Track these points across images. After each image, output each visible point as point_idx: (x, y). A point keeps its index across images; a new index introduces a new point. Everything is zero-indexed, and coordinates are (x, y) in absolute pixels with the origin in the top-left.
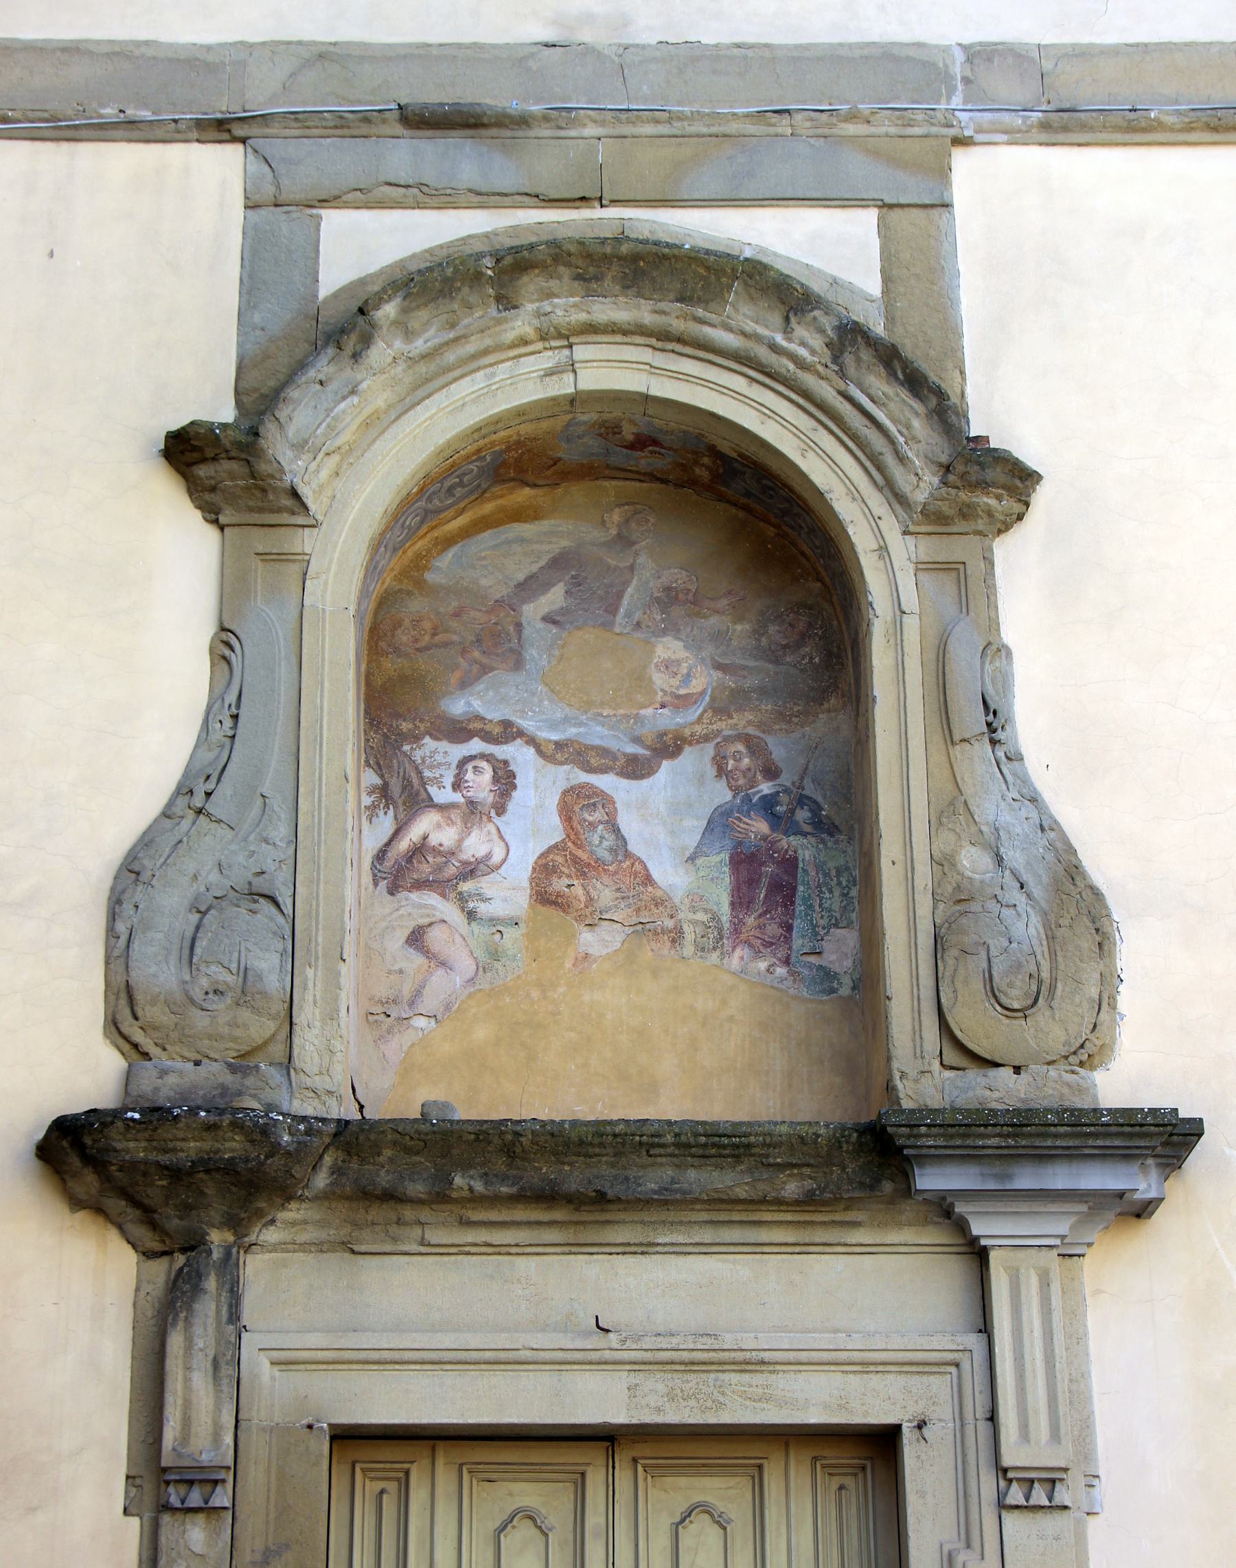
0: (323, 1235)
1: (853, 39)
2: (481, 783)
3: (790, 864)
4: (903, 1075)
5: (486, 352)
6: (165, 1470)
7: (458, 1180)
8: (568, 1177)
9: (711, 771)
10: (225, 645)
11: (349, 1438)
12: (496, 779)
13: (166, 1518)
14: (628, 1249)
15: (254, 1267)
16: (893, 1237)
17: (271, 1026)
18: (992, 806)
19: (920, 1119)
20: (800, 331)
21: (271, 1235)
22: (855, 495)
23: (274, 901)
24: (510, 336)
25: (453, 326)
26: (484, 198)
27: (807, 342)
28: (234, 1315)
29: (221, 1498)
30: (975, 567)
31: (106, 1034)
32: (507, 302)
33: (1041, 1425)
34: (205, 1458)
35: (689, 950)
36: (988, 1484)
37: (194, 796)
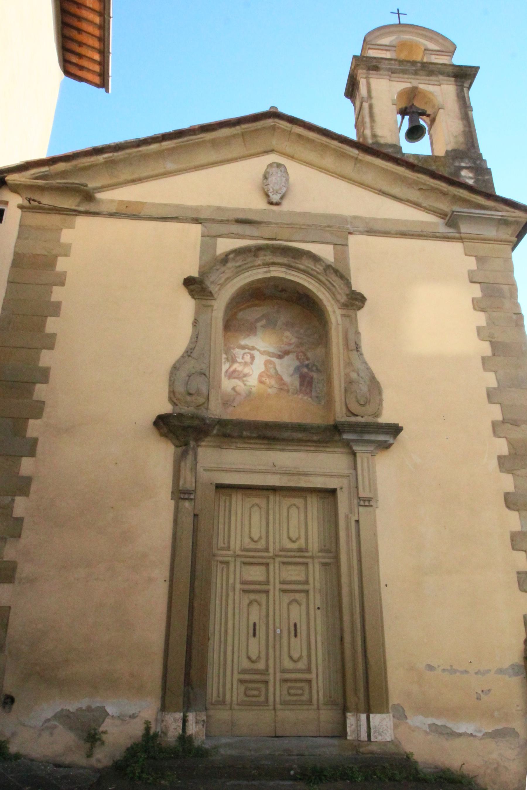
0: (215, 444)
1: (327, 213)
2: (248, 358)
3: (312, 378)
4: (338, 417)
5: (252, 267)
6: (180, 490)
7: (245, 433)
8: (268, 434)
9: (295, 358)
10: (195, 323)
11: (220, 487)
12: (251, 357)
13: (180, 500)
14: (280, 450)
15: (200, 450)
16: (336, 450)
17: (204, 400)
18: (357, 364)
19: (343, 424)
20: (318, 266)
21: (203, 444)
22: (329, 301)
23: (205, 375)
24: (257, 264)
25: (245, 260)
26: (252, 237)
27: (319, 268)
28: (196, 459)
29: (192, 497)
30: (353, 315)
31: (169, 400)
32: (256, 256)
33: (367, 489)
34: (189, 488)
35: (290, 394)
36: (356, 501)
37: (189, 353)
